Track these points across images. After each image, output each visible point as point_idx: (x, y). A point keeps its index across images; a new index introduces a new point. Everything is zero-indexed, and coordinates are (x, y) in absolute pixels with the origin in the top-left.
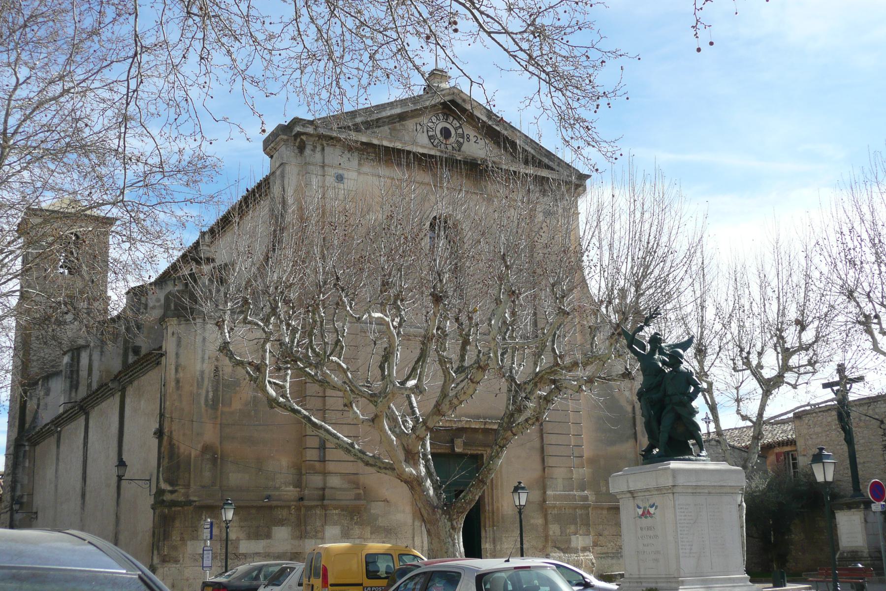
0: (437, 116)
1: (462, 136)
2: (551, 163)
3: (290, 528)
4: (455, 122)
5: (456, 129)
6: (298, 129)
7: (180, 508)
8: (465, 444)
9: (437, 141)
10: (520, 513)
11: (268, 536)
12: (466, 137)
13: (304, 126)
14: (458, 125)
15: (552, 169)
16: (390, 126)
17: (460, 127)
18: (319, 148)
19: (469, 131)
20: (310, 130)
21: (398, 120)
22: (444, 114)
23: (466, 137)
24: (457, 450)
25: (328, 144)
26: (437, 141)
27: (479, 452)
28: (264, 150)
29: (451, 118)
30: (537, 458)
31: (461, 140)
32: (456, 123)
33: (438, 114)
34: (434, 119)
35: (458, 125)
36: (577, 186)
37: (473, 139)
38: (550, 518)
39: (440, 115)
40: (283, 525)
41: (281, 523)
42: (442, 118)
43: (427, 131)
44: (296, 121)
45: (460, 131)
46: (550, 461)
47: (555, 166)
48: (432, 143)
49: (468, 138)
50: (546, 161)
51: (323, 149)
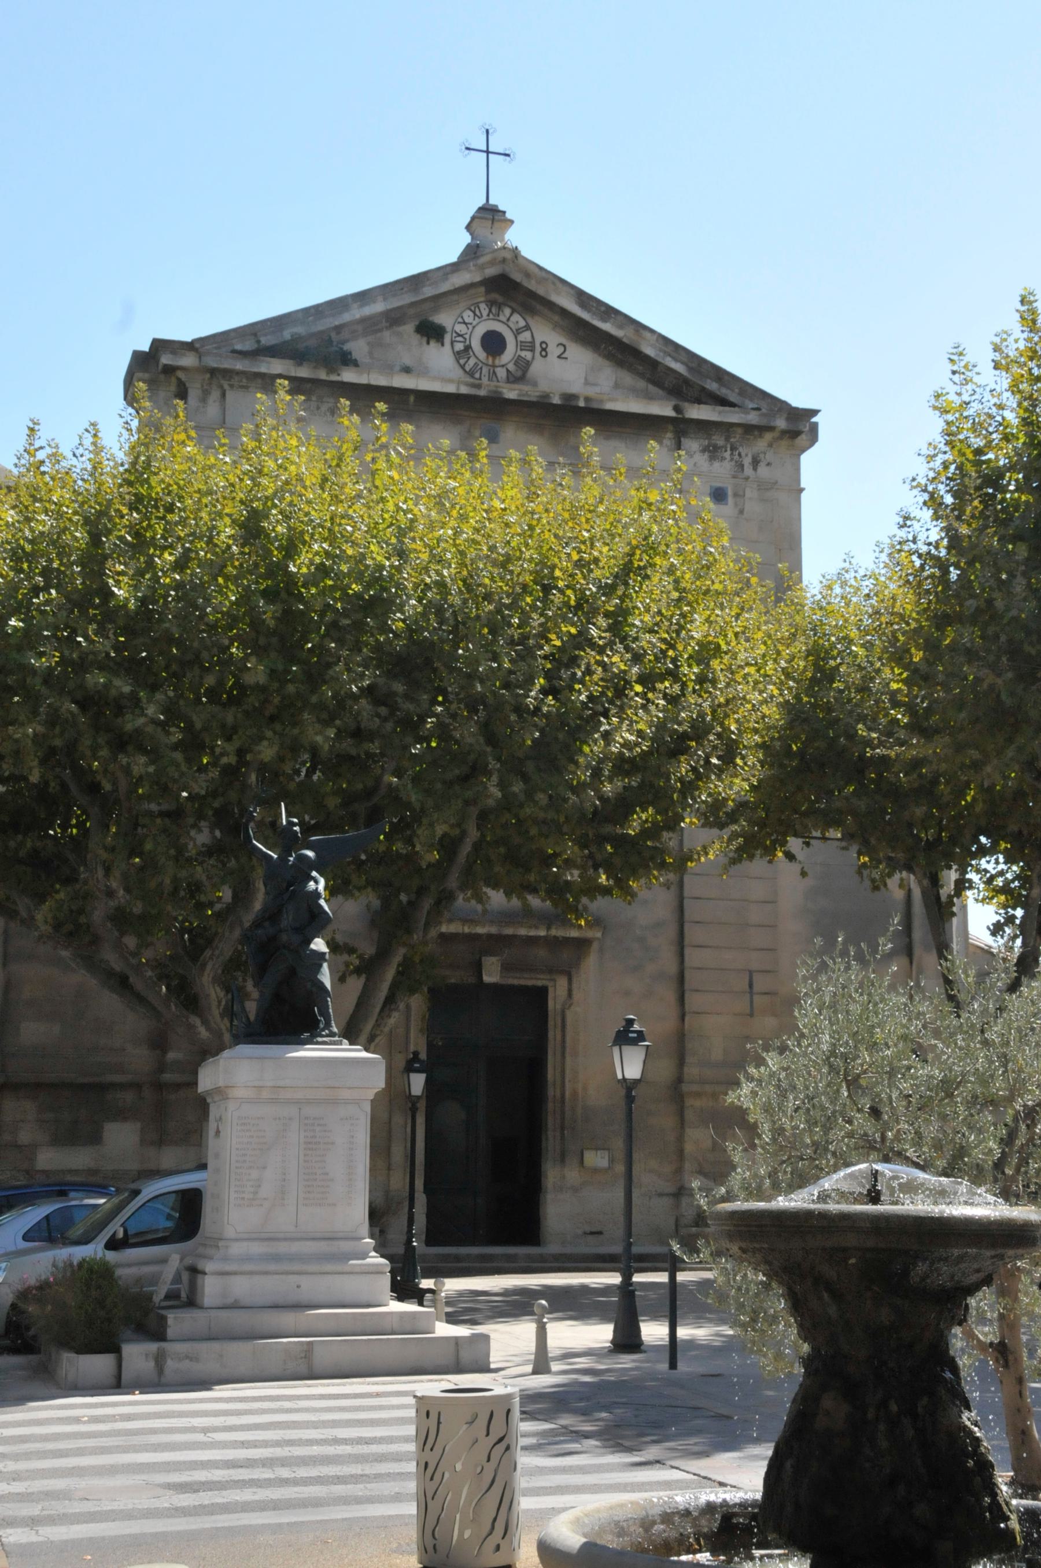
0: (474, 309)
1: (530, 346)
2: (724, 392)
3: (139, 1125)
4: (516, 317)
5: (517, 333)
6: (166, 359)
7: (846, 1094)
8: (507, 968)
9: (472, 361)
10: (630, 1099)
11: (95, 1138)
12: (538, 349)
13: (174, 352)
14: (522, 323)
15: (732, 405)
16: (370, 338)
17: (527, 327)
18: (215, 394)
19: (545, 333)
20: (188, 361)
21: (384, 324)
22: (491, 304)
23: (538, 349)
24: (487, 979)
25: (231, 386)
26: (472, 361)
27: (539, 983)
28: (125, 399)
29: (507, 311)
30: (669, 995)
31: (527, 355)
32: (518, 321)
33: (477, 305)
34: (468, 316)
35: (522, 323)
36: (793, 434)
37: (554, 351)
38: (689, 1115)
39: (483, 306)
40: (125, 1119)
41: (121, 1115)
42: (485, 313)
43: (452, 343)
44: (159, 345)
45: (526, 336)
46: (693, 1001)
47: (733, 397)
48: (463, 367)
49: (544, 350)
50: (712, 386)
51: (223, 395)
